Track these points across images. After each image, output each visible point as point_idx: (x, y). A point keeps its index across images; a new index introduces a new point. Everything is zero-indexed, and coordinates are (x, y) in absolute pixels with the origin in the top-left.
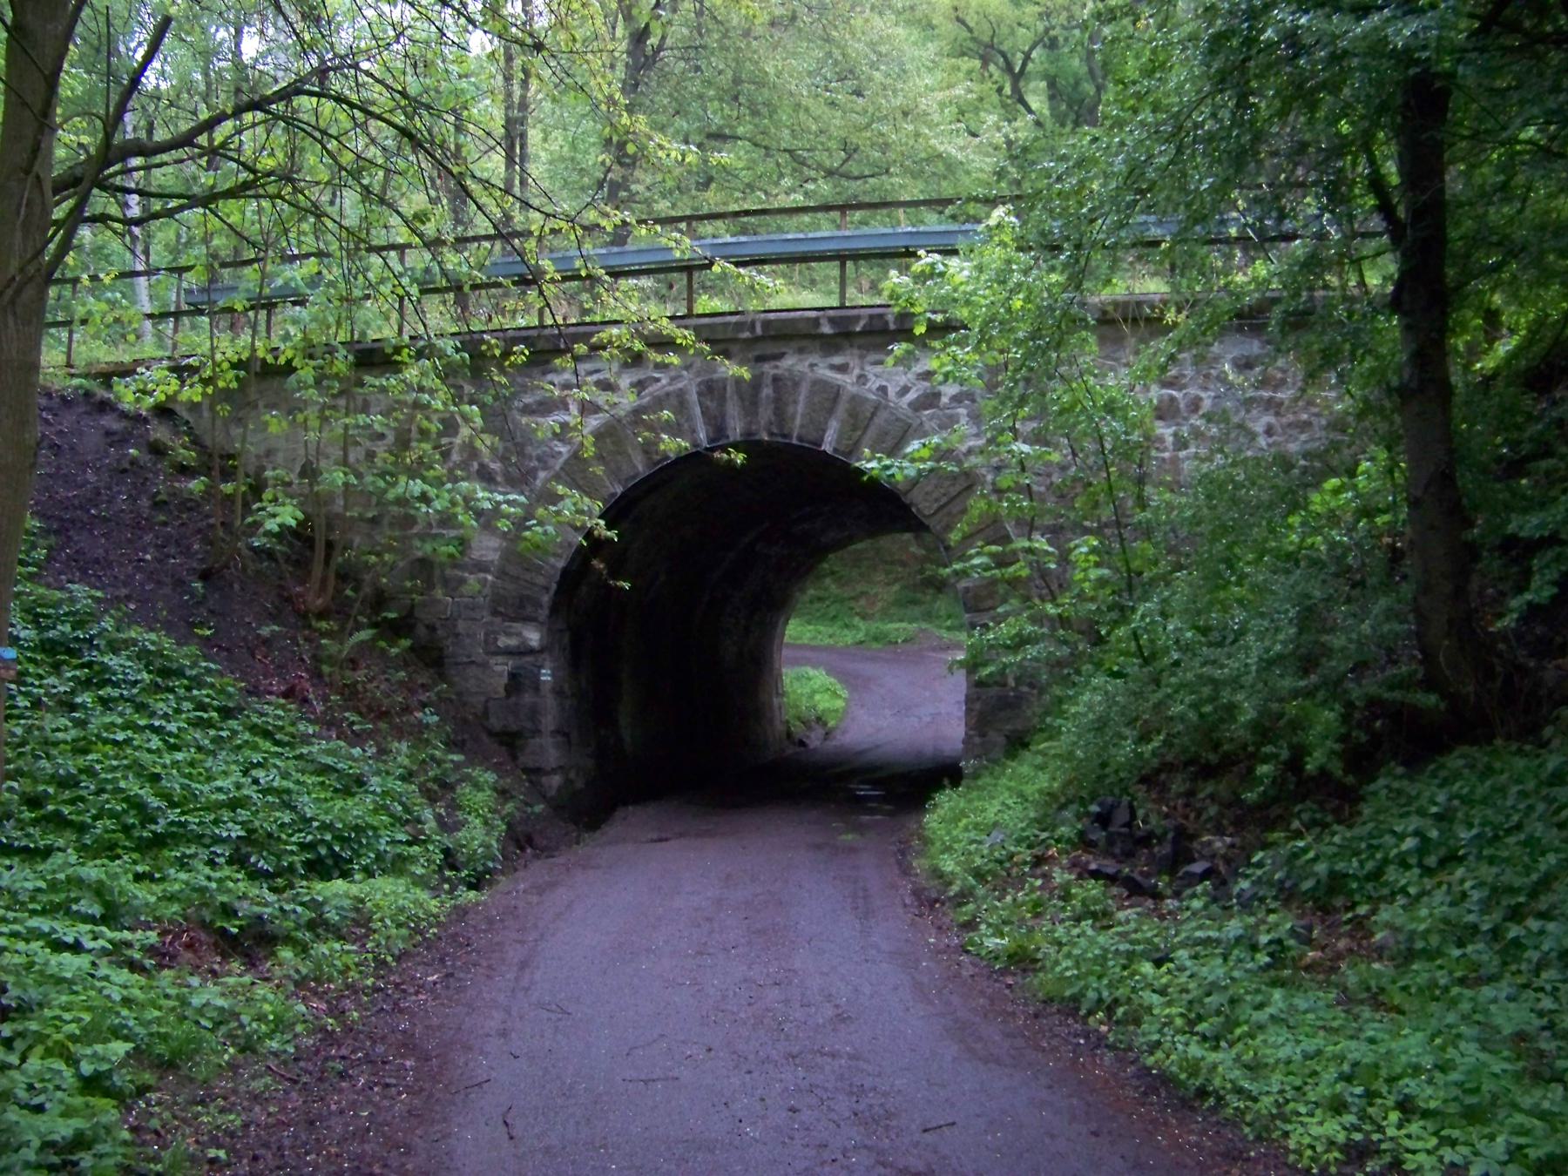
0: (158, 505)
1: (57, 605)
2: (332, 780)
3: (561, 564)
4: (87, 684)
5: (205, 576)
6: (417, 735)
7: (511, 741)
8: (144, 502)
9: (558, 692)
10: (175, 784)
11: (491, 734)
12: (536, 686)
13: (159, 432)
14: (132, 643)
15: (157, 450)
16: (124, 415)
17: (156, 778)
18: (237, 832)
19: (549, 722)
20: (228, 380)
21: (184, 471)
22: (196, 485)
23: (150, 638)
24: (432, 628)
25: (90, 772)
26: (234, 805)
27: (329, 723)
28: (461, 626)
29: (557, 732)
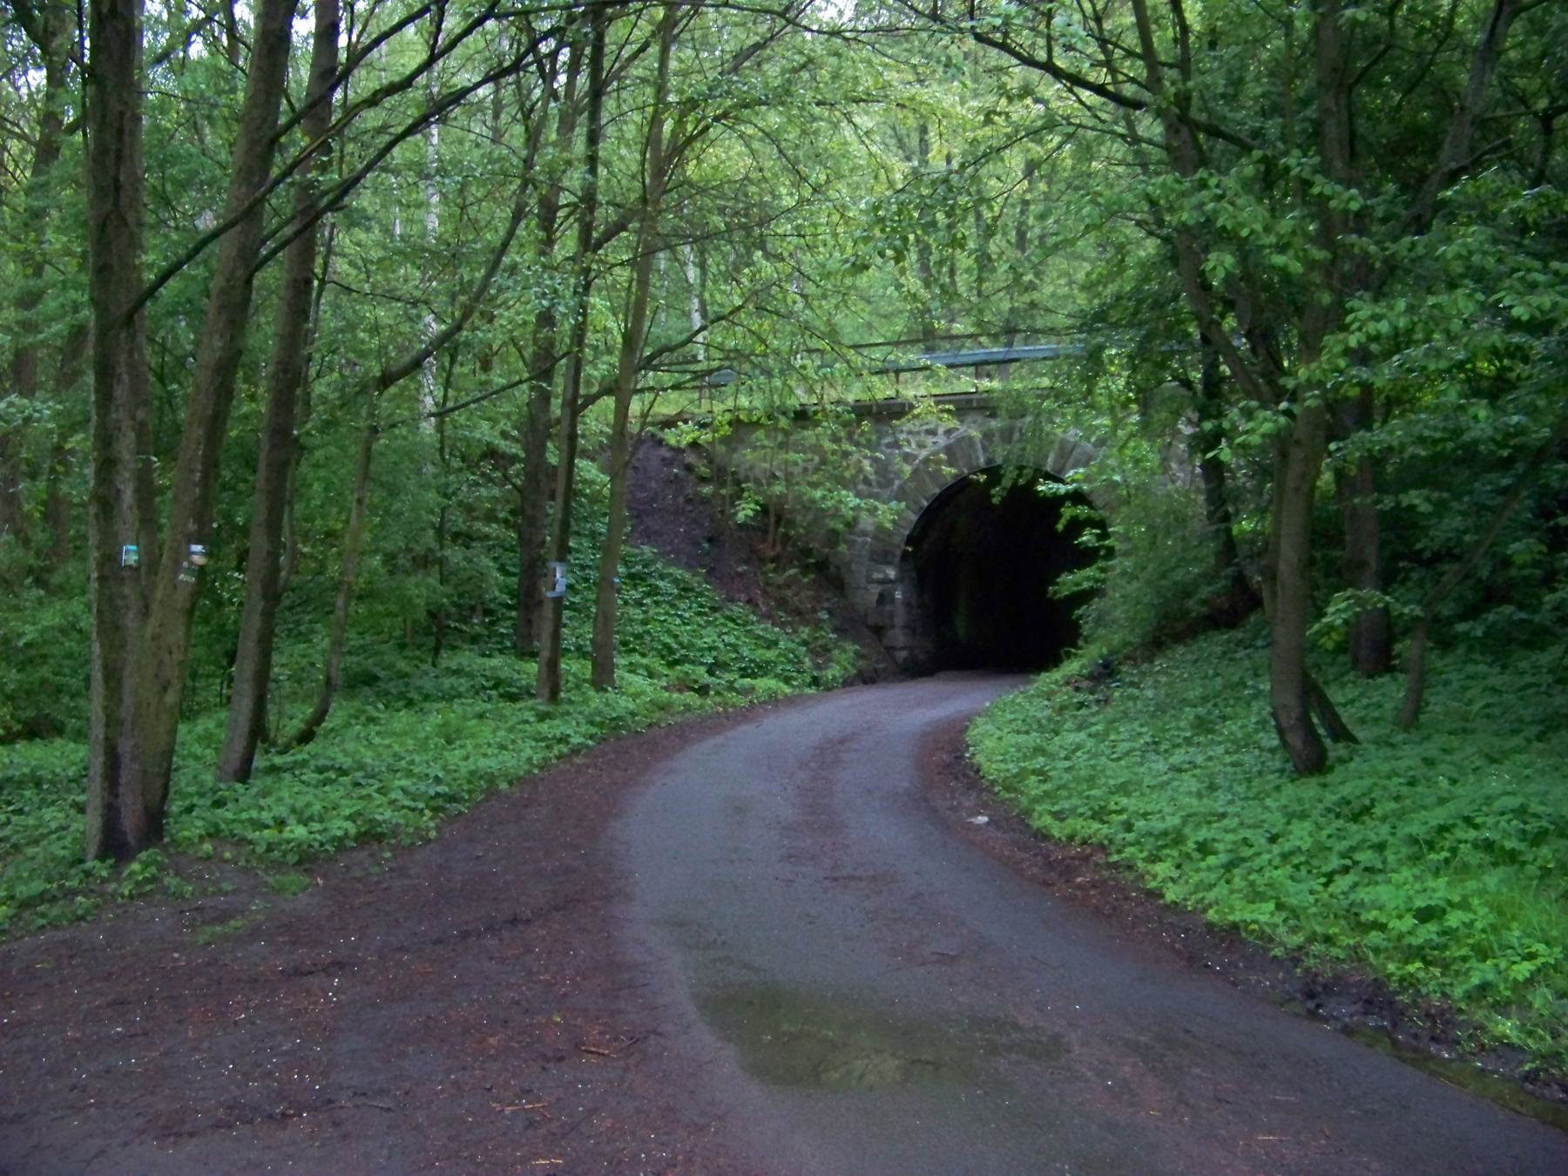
0: (689, 501)
1: (636, 555)
2: (761, 642)
3: (907, 533)
4: (648, 594)
5: (710, 540)
6: (817, 625)
7: (878, 631)
8: (681, 499)
9: (908, 605)
10: (685, 639)
11: (868, 627)
12: (893, 600)
13: (690, 458)
14: (671, 575)
15: (689, 468)
16: (672, 448)
17: (676, 637)
18: (711, 661)
19: (899, 620)
20: (727, 430)
21: (704, 480)
22: (707, 490)
23: (678, 572)
24: (838, 567)
25: (648, 633)
26: (711, 649)
27: (768, 616)
28: (854, 567)
29: (906, 627)
